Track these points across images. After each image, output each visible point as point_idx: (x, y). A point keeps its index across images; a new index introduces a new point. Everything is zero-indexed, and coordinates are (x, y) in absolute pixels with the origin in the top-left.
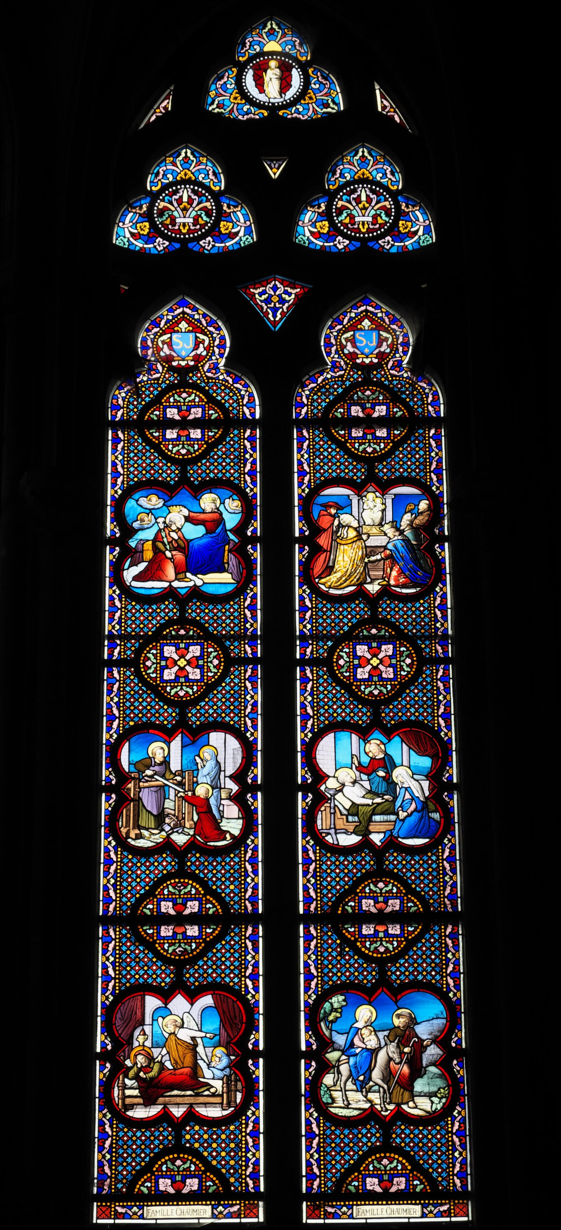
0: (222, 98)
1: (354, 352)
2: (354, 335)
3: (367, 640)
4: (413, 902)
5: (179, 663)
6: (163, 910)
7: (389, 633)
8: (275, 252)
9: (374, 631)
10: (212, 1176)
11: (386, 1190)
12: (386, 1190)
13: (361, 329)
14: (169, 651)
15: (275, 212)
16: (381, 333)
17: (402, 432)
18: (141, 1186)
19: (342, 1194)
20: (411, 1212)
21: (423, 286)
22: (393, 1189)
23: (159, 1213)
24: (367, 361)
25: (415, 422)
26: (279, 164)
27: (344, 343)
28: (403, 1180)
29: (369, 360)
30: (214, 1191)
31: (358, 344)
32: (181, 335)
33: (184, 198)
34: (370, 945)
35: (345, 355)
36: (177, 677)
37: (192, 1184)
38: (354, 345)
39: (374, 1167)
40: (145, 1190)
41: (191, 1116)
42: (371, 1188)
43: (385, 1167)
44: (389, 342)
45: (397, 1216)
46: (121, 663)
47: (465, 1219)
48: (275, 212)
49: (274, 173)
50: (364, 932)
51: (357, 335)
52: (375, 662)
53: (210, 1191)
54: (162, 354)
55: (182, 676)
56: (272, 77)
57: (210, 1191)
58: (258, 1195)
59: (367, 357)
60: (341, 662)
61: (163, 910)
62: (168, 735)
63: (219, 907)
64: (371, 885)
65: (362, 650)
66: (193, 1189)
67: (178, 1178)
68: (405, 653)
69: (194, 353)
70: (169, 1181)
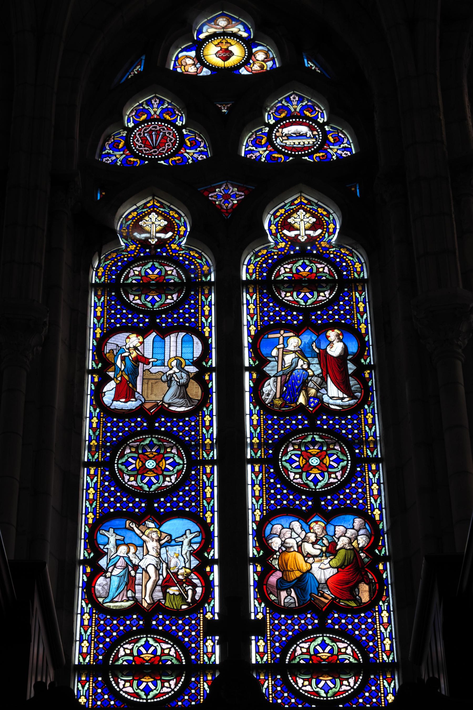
0: (185, 62)
8: (225, 163)
15: (224, 136)
25: (344, 284)
26: (226, 103)
33: (149, 127)
46: (96, 464)
48: (224, 136)
56: (223, 47)
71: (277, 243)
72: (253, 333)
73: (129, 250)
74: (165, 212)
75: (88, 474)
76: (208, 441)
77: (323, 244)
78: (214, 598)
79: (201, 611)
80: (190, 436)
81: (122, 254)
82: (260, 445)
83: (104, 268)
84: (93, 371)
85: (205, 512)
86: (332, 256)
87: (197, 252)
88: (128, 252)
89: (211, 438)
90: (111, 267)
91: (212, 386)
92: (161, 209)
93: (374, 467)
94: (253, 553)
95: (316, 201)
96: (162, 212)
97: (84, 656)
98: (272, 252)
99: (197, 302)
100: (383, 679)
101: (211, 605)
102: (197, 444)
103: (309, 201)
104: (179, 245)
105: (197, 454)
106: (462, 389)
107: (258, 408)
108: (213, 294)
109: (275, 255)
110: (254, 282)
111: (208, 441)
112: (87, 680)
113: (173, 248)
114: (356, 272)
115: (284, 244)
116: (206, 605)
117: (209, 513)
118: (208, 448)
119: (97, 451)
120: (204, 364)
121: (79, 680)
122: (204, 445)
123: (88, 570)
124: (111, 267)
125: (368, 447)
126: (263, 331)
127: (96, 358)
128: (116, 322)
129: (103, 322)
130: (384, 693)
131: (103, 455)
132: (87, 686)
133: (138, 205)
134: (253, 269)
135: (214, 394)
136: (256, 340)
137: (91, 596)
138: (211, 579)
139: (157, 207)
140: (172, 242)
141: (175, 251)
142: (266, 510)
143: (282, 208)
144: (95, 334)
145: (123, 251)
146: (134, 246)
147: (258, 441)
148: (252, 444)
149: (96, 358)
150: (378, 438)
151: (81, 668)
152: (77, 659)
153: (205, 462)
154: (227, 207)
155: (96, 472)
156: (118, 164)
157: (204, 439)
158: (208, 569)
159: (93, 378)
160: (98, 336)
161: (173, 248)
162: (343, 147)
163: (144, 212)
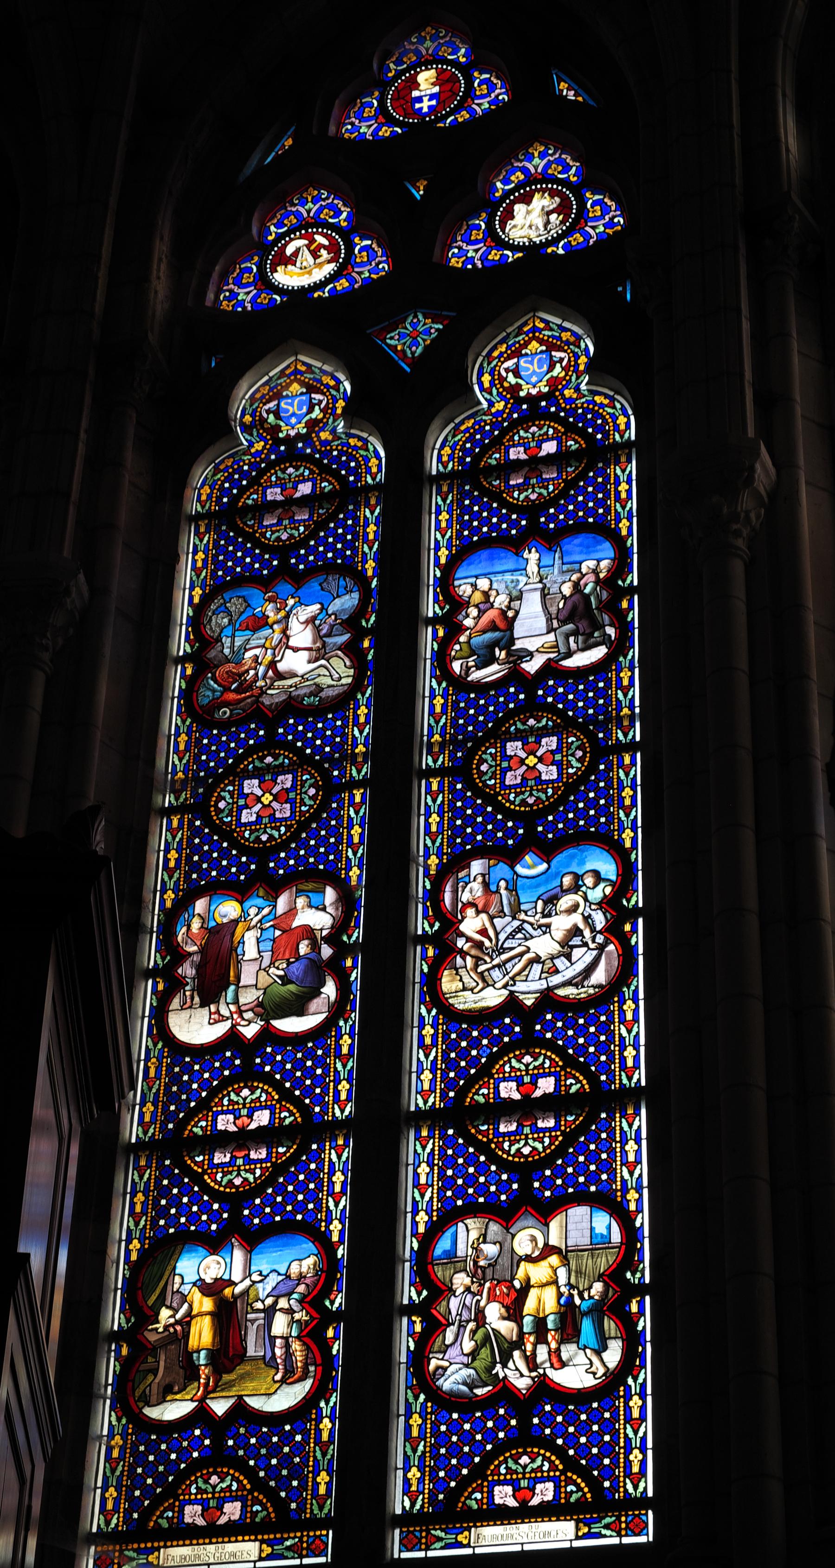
1: (517, 384)
2: (278, 405)
3: (258, 774)
4: (289, 1111)
5: (271, 798)
6: (503, 1094)
7: (553, 721)
9: (269, 759)
10: (575, 1477)
11: (524, 1503)
12: (524, 1503)
13: (287, 397)
14: (251, 786)
16: (553, 353)
17: (328, 509)
18: (158, 1517)
19: (452, 1512)
20: (559, 1534)
21: (213, 364)
22: (535, 1501)
23: (492, 1539)
24: (534, 392)
25: (599, 454)
27: (265, 415)
28: (550, 1485)
29: (296, 431)
30: (577, 1500)
31: (522, 373)
32: (294, 399)
34: (510, 1146)
35: (505, 389)
36: (524, 779)
37: (545, 1492)
38: (517, 374)
39: (507, 1468)
40: (164, 1524)
41: (240, 1410)
42: (501, 1502)
43: (214, 1487)
44: (564, 364)
45: (510, 1542)
47: (322, 1560)
49: (418, 195)
50: (503, 1129)
51: (283, 405)
52: (267, 799)
53: (572, 1500)
54: (506, 385)
55: (532, 778)
57: (572, 1500)
58: (643, 1502)
59: (534, 387)
60: (222, 805)
61: (503, 1094)
62: (241, 893)
63: (585, 1082)
64: (232, 1094)
65: (514, 748)
66: (546, 1499)
67: (524, 1483)
68: (576, 744)
69: (549, 376)
70: (509, 1489)
71: (491, 404)
72: (443, 561)
73: (493, 410)
74: (554, 337)
75: (429, 791)
76: (626, 711)
77: (324, 435)
78: (637, 975)
79: (616, 999)
80: (596, 706)
81: (241, 460)
82: (442, 745)
83: (453, 448)
84: (434, 621)
85: (622, 830)
86: (335, 453)
87: (606, 396)
88: (492, 414)
89: (631, 707)
90: (465, 443)
91: (633, 619)
92: (308, 376)
93: (627, 760)
94: (423, 929)
95: (319, 364)
96: (549, 337)
97: (425, 1095)
98: (482, 420)
99: (607, 478)
100: (620, 1118)
101: (633, 988)
102: (608, 719)
103: (309, 366)
104: (577, 389)
105: (608, 734)
106: (34, 719)
107: (444, 685)
108: (634, 462)
109: (486, 424)
110: (208, 516)
111: (626, 711)
112: (431, 1136)
113: (323, 438)
114: (619, 431)
115: (503, 403)
116: (625, 989)
117: (628, 831)
118: (360, 759)
119: (442, 751)
120: (620, 583)
121: (418, 1138)
122: (619, 720)
123: (431, 953)
124: (222, 484)
125: (620, 726)
126: (214, 591)
127: (441, 598)
128: (472, 534)
129: (451, 537)
130: (620, 1142)
131: (194, 794)
132: (430, 1146)
133: (271, 374)
134: (449, 456)
135: (636, 631)
136: (199, 611)
137: (435, 997)
138: (633, 943)
139: (540, 330)
140: (565, 387)
141: (570, 401)
142: (183, 890)
143: (501, 342)
144: (191, 598)
145: (245, 454)
146: (262, 443)
147: (364, 750)
148: (430, 745)
149: (441, 598)
150: (637, 710)
151: (420, 1117)
152: (416, 1102)
153: (620, 748)
154: (413, 353)
155: (181, 822)
156: (249, 308)
157: (619, 707)
158: (628, 927)
159: (435, 632)
160: (443, 561)
161: (323, 438)
162: (604, 218)
163: (519, 342)
